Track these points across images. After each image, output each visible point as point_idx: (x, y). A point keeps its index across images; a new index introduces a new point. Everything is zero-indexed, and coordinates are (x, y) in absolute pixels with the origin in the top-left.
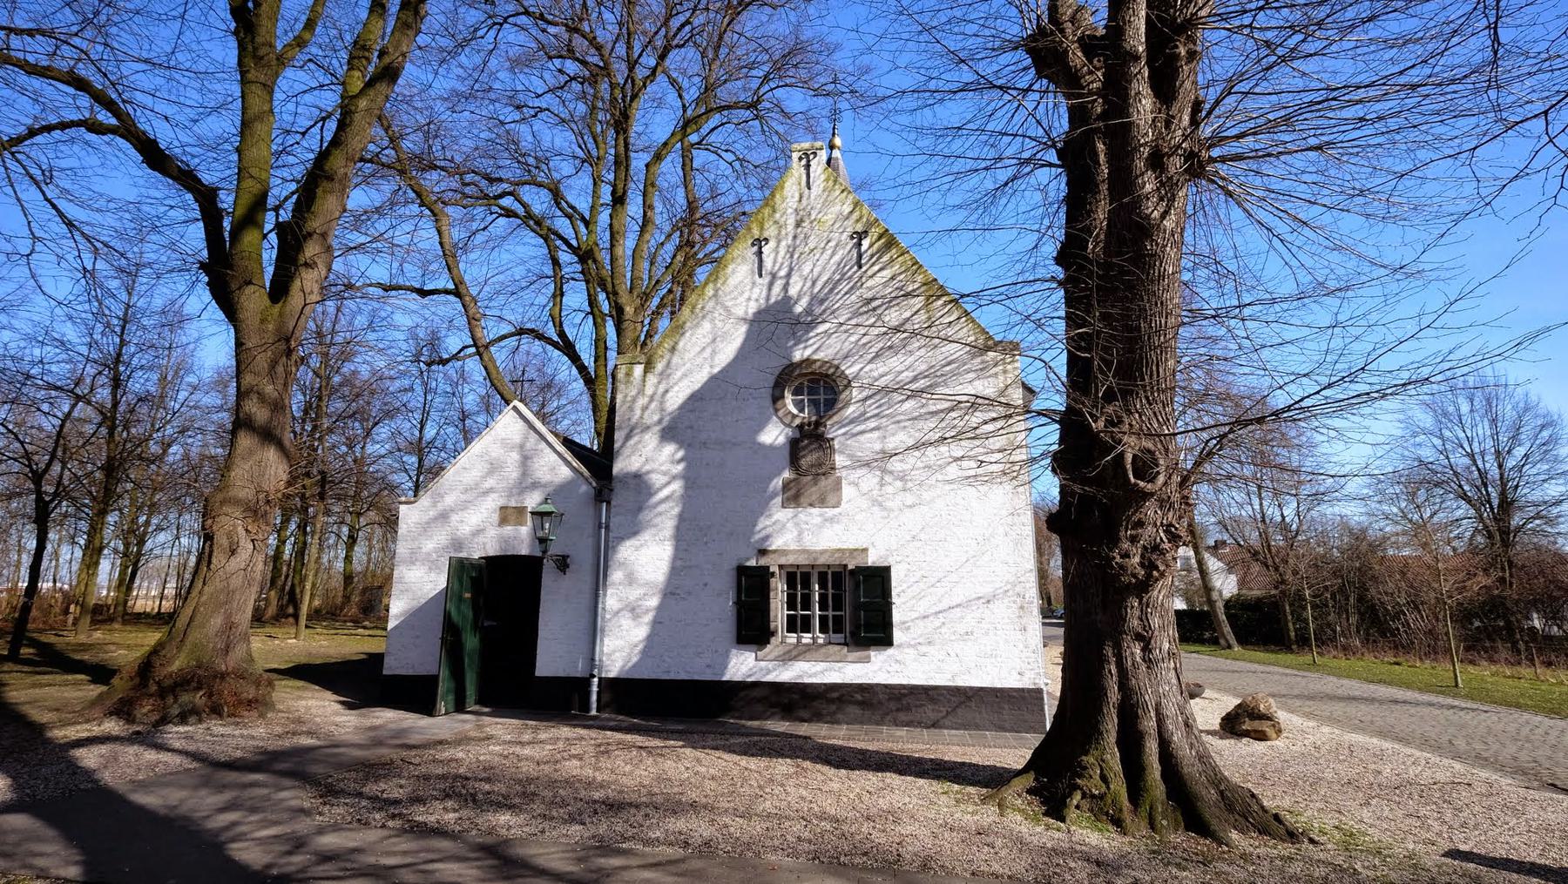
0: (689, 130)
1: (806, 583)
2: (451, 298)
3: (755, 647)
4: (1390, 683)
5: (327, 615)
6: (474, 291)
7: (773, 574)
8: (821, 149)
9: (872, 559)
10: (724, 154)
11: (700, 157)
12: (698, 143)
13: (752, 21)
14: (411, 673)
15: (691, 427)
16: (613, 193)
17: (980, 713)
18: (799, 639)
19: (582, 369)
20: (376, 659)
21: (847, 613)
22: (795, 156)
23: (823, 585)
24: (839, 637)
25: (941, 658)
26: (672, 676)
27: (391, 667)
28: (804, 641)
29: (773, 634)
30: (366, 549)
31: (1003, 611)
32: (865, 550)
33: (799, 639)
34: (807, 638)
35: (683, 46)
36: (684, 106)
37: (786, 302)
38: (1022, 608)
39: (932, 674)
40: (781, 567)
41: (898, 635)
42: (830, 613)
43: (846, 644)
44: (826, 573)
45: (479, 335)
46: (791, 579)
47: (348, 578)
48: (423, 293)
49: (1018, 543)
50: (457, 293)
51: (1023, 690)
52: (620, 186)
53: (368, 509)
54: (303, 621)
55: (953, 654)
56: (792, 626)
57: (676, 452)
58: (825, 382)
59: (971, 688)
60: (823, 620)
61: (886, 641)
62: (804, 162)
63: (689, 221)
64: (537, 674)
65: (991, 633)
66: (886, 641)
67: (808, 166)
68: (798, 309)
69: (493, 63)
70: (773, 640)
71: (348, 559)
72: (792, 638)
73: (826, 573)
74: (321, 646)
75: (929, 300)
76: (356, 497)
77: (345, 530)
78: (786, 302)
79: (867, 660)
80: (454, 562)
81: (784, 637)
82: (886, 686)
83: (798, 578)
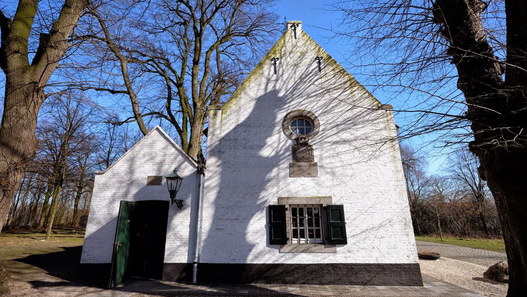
0: (223, 41)
1: (301, 214)
2: (126, 95)
3: (278, 246)
4: (488, 249)
5: (59, 228)
6: (135, 92)
7: (287, 209)
8: (300, 24)
9: (335, 201)
10: (231, 56)
11: (222, 57)
12: (223, 51)
13: (245, 8)
14: (96, 262)
15: (245, 139)
16: (194, 60)
17: (391, 276)
18: (299, 241)
19: (177, 127)
20: (78, 250)
21: (306, 228)
22: (289, 25)
23: (310, 214)
24: (319, 240)
25: (371, 250)
26: (237, 262)
27: (86, 258)
28: (301, 242)
29: (288, 239)
30: (84, 202)
31: (398, 227)
32: (330, 197)
33: (299, 241)
34: (303, 241)
35: (224, 7)
36: (218, 37)
37: (275, 92)
38: (405, 224)
39: (367, 258)
40: (290, 205)
41: (349, 240)
42: (314, 228)
43: (323, 243)
44: (296, 209)
45: (137, 109)
46: (294, 211)
47: (76, 211)
48: (113, 92)
49: (400, 194)
50: (128, 93)
51: (410, 264)
52: (197, 58)
53: (85, 186)
54: (50, 231)
55: (376, 248)
56: (295, 235)
57: (217, 161)
58: (306, 121)
59: (386, 264)
60: (310, 231)
61: (343, 241)
62: (293, 28)
63: (220, 79)
64: (165, 262)
65: (393, 236)
66: (343, 241)
67: (295, 30)
68: (281, 94)
69: (146, 14)
70: (288, 241)
71: (76, 206)
72: (295, 241)
73: (296, 209)
74: (57, 243)
75: (351, 86)
76: (81, 181)
77: (76, 194)
78: (275, 92)
79: (335, 252)
80: (122, 204)
81: (292, 240)
82: (344, 264)
83: (298, 211)
